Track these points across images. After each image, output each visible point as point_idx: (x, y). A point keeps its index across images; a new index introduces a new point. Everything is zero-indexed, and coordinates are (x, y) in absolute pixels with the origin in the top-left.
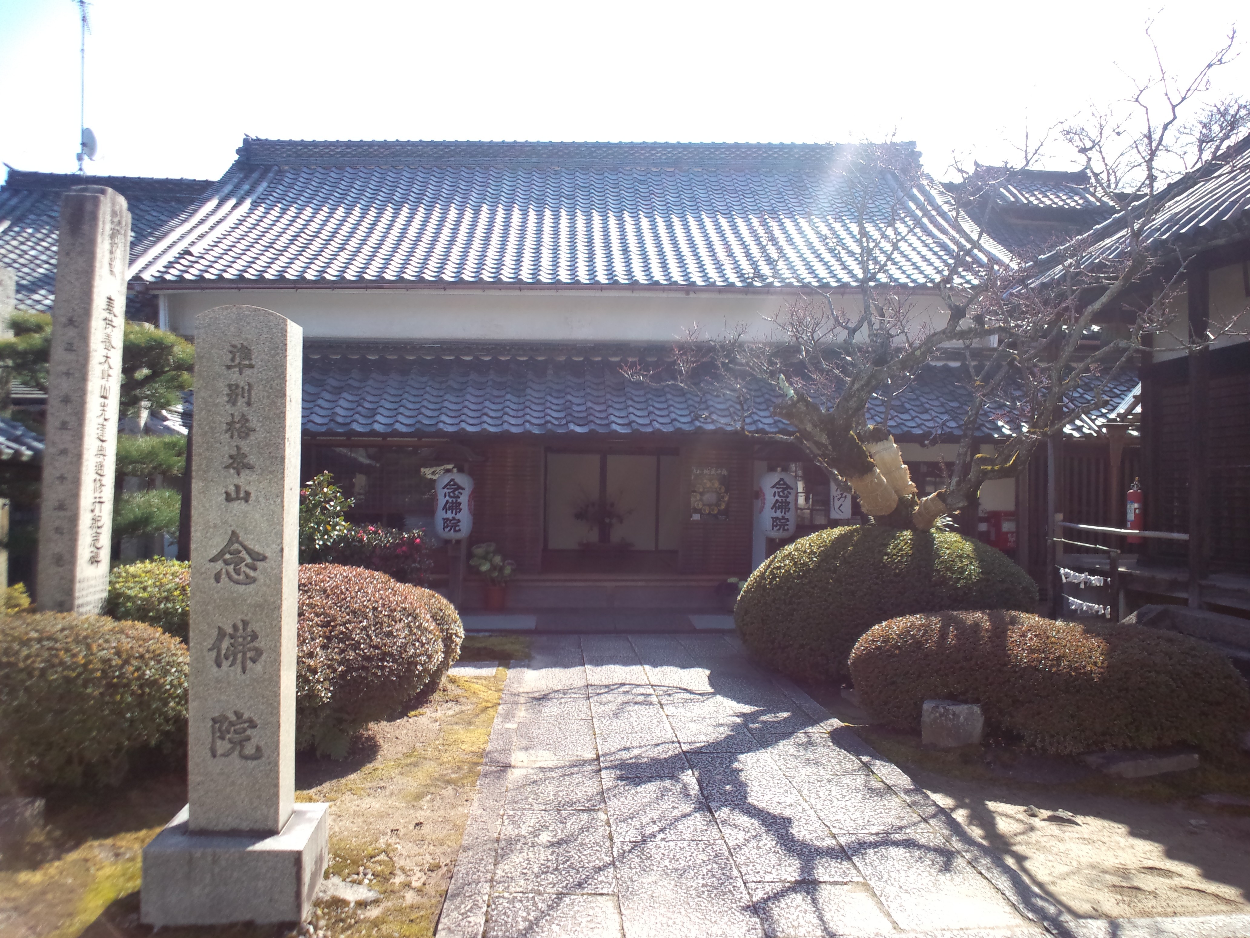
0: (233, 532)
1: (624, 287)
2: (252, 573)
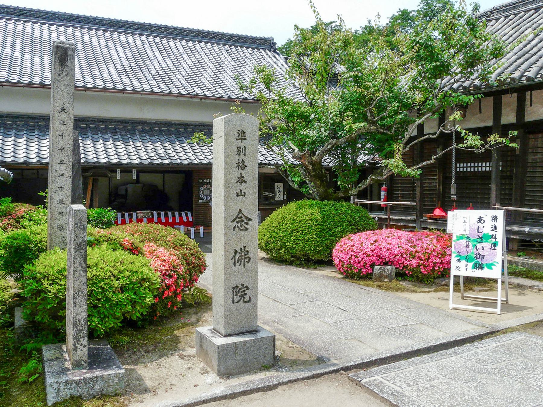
0: (240, 210)
1: (90, 90)
2: (247, 226)
